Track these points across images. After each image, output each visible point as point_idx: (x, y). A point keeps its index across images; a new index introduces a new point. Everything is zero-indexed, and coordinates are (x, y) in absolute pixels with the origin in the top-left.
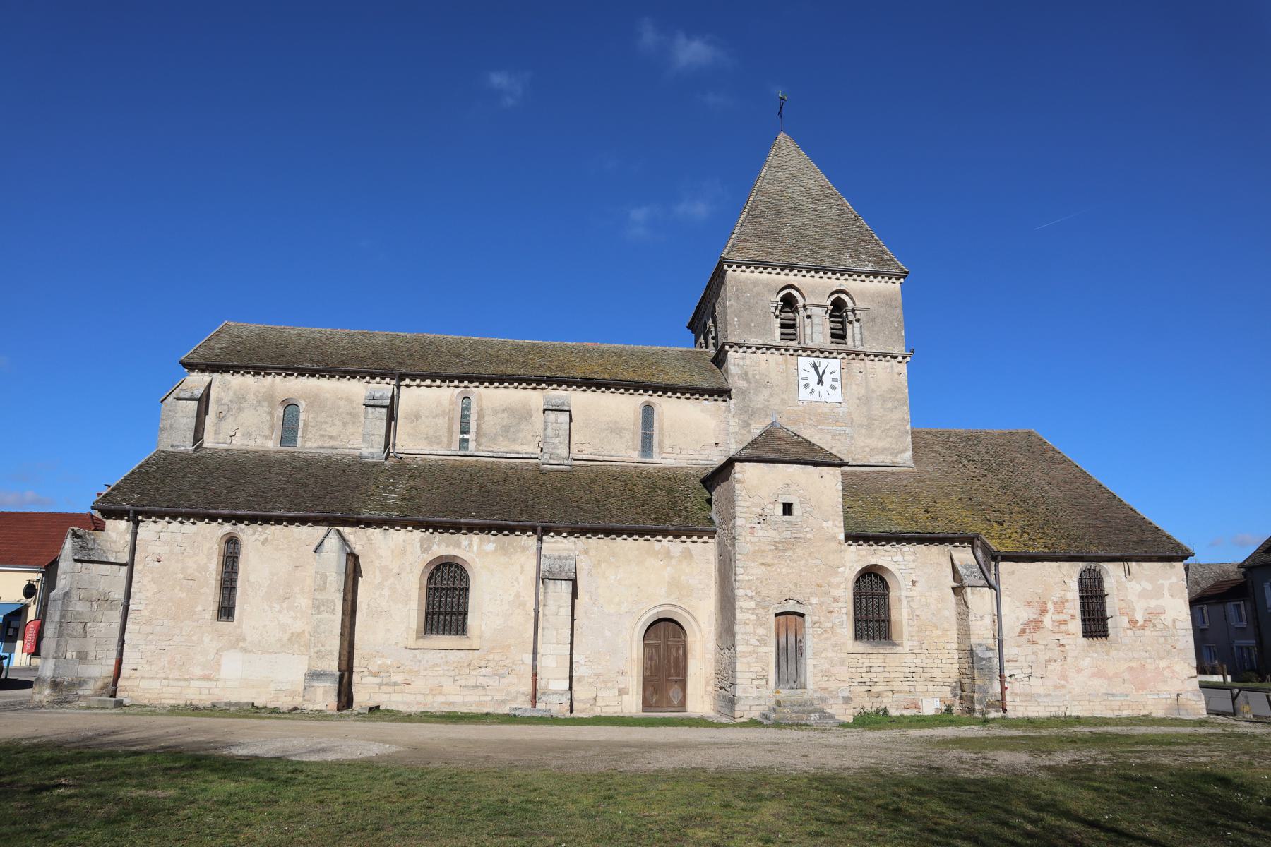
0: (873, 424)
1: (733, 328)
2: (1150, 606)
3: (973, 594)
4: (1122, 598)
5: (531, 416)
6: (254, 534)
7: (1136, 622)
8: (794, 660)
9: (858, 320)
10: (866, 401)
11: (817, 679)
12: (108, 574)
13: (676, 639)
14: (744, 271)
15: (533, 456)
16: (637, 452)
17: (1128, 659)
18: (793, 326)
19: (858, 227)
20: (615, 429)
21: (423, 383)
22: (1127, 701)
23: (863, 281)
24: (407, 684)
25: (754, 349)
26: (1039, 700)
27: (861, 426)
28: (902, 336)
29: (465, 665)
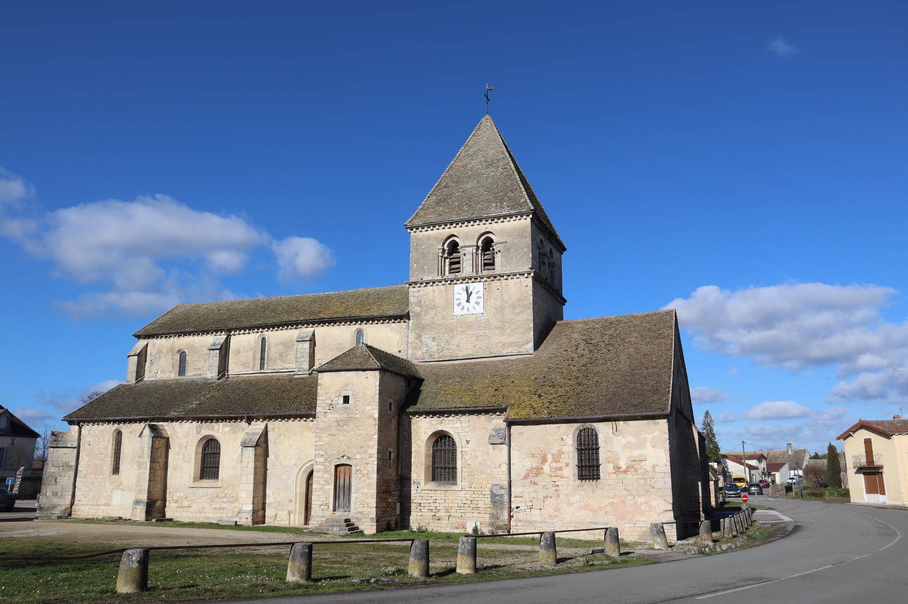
0: (505, 326)
2: (633, 455)
3: (494, 449)
4: (609, 450)
6: (126, 429)
7: (620, 468)
8: (348, 493)
10: (500, 310)
12: (68, 453)
14: (421, 231)
17: (611, 497)
21: (236, 333)
26: (536, 526)
27: (496, 328)
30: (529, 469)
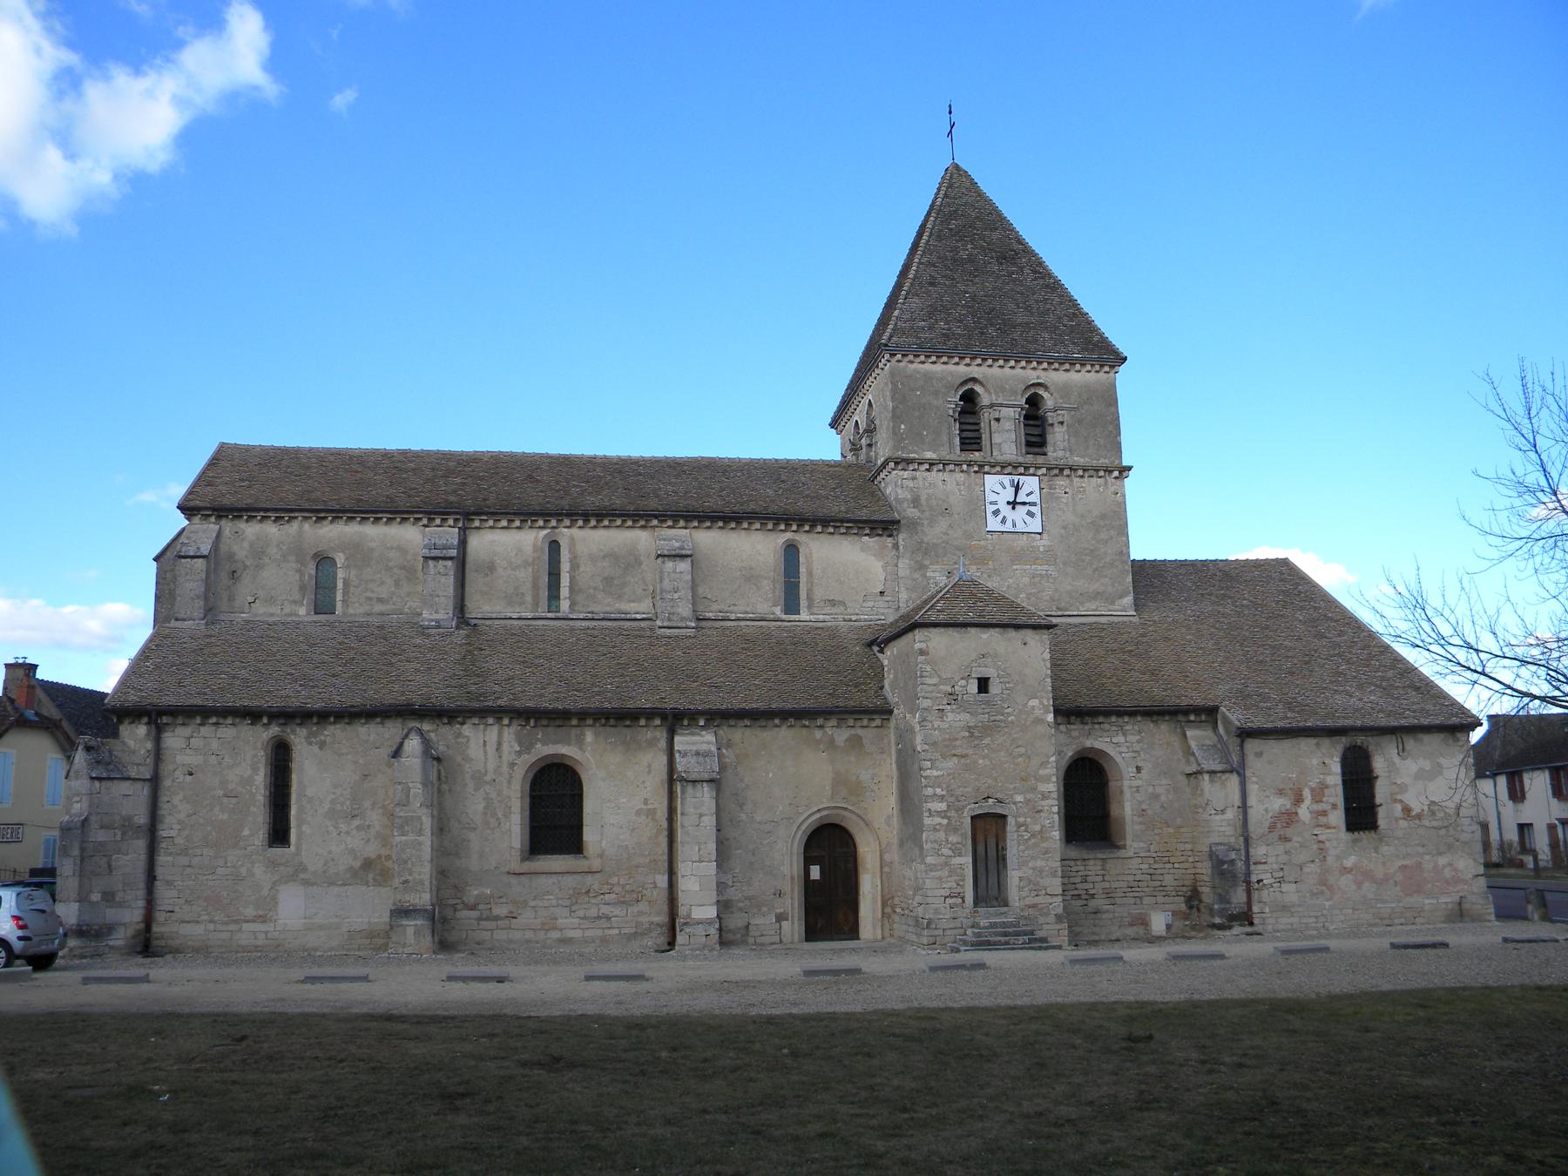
5: (640, 564)
11: (1024, 894)
14: (912, 362)
16: (779, 607)
20: (751, 577)
24: (513, 918)
29: (584, 891)
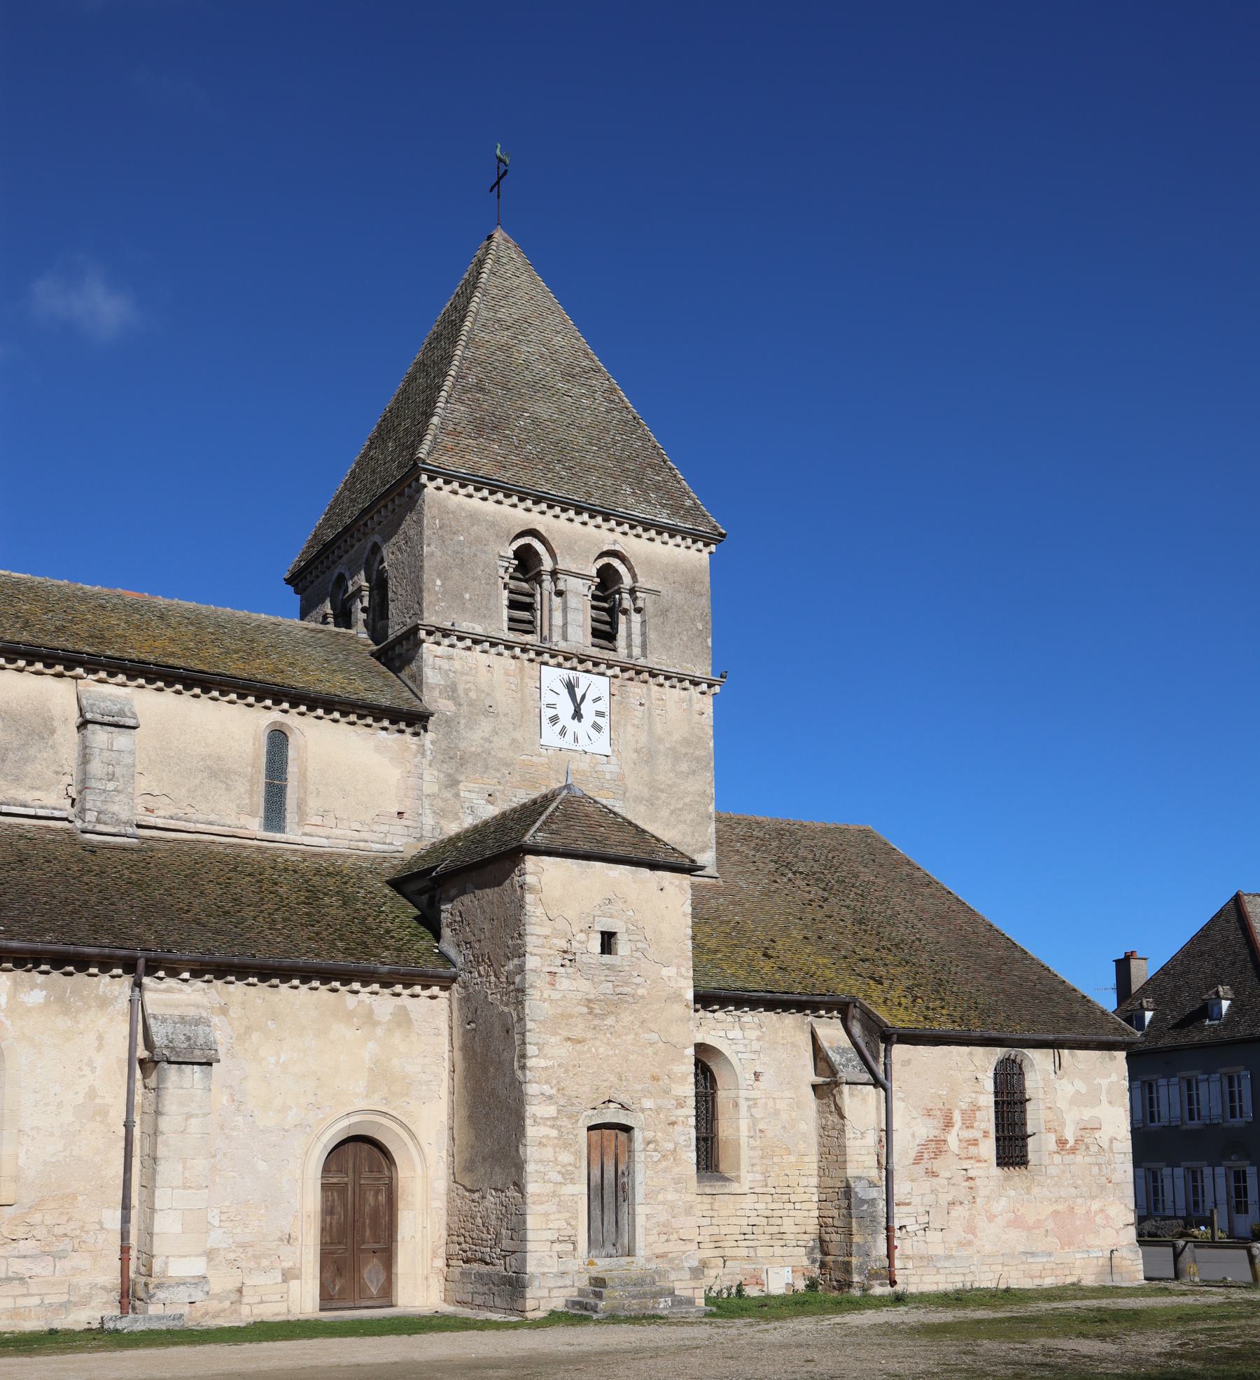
0: (658, 798)
1: (433, 599)
3: (851, 1095)
4: (1049, 1105)
5: (53, 732)
9: (638, 610)
10: (647, 756)
11: (651, 1239)
13: (377, 1175)
15: (57, 814)
18: (529, 607)
19: (639, 438)
20: (217, 772)
22: (1050, 1262)
23: (651, 540)
25: (468, 642)
26: (939, 1266)
28: (708, 647)
30: (923, 1142)
